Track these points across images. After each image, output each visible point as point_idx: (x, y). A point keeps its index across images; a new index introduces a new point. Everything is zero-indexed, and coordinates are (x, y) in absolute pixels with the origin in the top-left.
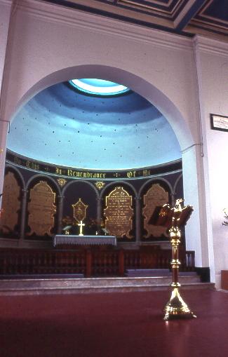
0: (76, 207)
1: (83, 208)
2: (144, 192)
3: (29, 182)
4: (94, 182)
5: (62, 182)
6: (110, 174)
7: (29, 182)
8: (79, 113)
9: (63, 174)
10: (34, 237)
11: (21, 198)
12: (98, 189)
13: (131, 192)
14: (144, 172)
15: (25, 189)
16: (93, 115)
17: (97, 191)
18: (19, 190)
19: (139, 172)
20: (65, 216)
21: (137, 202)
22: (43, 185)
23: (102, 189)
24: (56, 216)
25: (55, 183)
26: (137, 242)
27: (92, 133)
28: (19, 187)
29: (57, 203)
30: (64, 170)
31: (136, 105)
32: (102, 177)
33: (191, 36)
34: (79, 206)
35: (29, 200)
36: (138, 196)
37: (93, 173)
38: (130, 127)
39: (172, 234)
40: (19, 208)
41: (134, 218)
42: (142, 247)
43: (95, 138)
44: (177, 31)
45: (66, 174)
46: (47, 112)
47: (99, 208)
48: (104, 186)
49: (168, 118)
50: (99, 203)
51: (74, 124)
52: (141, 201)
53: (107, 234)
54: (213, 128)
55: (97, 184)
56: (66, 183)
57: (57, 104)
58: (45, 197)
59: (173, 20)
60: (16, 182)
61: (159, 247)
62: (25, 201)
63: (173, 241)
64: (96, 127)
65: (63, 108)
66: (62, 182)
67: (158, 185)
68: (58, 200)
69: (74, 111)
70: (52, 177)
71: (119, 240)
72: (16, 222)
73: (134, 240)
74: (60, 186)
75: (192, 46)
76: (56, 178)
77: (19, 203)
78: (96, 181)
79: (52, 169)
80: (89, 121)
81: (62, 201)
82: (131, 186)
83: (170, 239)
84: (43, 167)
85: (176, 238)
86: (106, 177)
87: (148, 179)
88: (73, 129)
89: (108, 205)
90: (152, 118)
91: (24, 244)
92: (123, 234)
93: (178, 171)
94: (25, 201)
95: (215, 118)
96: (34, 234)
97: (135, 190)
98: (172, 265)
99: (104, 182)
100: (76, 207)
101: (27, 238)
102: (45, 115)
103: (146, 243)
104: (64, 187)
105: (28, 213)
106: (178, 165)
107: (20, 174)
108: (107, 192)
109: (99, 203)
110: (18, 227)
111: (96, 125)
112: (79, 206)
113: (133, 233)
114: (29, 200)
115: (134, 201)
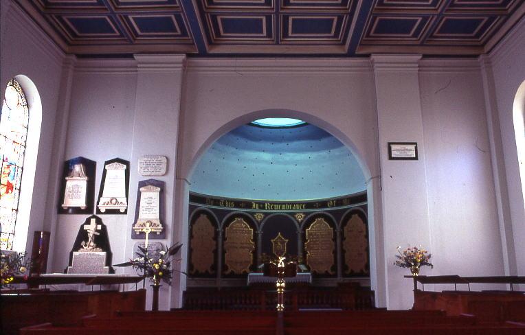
0: (276, 243)
1: (283, 243)
2: (227, 224)
3: (223, 221)
4: (293, 214)
5: (259, 217)
6: (310, 205)
7: (223, 221)
8: (269, 145)
9: (260, 208)
10: (232, 275)
11: (216, 238)
12: (298, 221)
13: (332, 224)
14: (345, 202)
15: (220, 229)
16: (283, 145)
17: (297, 224)
18: (213, 230)
19: (339, 201)
20: (265, 250)
21: (338, 234)
22: (238, 222)
23: (302, 221)
24: (255, 252)
25: (252, 218)
26: (339, 278)
27: (286, 163)
28: (213, 228)
29: (255, 240)
30: (262, 205)
31: (314, 133)
32: (302, 208)
33: (368, 56)
34: (280, 241)
35: (224, 239)
36: (338, 227)
37: (293, 204)
38: (324, 153)
39: (278, 285)
40: (214, 248)
41: (335, 252)
42: (340, 285)
43: (291, 167)
44: (351, 54)
45: (264, 208)
46: (234, 150)
47: (300, 242)
48: (305, 217)
49: (484, 72)
50: (299, 236)
51: (266, 156)
52: (342, 234)
53: (305, 271)
54: (391, 158)
55: (296, 216)
56: (264, 218)
57: (242, 141)
58: (242, 232)
59: (344, 43)
60: (210, 223)
61: (358, 284)
62: (220, 240)
63: (279, 290)
64: (290, 156)
65: (250, 143)
66: (259, 217)
67: (205, 216)
68: (255, 235)
69: (262, 144)
70: (246, 212)
71: (315, 275)
72: (212, 261)
73: (335, 276)
74: (257, 221)
75: (371, 67)
76: (253, 214)
77: (214, 242)
78: (295, 213)
79: (248, 204)
80: (280, 151)
81: (260, 236)
82: (331, 216)
83: (276, 288)
84: (238, 203)
85: (281, 287)
86: (306, 208)
87: (348, 209)
88: (266, 162)
89: (309, 238)
90: (334, 147)
91: (221, 283)
92: (323, 269)
93: (364, 204)
94: (220, 240)
95: (394, 147)
96: (232, 272)
97: (335, 220)
98: (277, 309)
99: (304, 213)
100: (276, 243)
101: (224, 276)
102: (232, 153)
103: (347, 280)
104: (261, 221)
105: (224, 252)
106: (362, 197)
107: (215, 215)
108: (307, 225)
109: (299, 236)
110: (214, 267)
111: (288, 154)
112: (280, 241)
113: (334, 268)
114: (224, 239)
115: (335, 233)
